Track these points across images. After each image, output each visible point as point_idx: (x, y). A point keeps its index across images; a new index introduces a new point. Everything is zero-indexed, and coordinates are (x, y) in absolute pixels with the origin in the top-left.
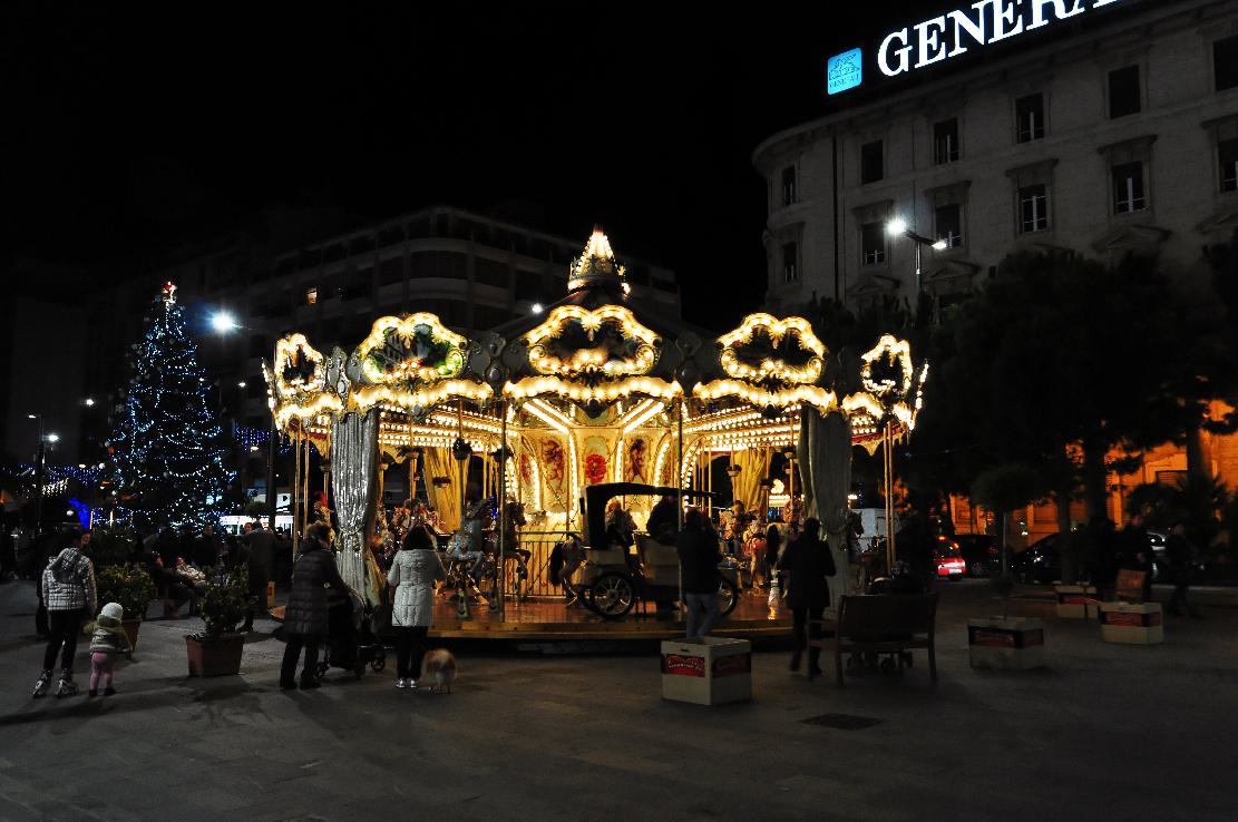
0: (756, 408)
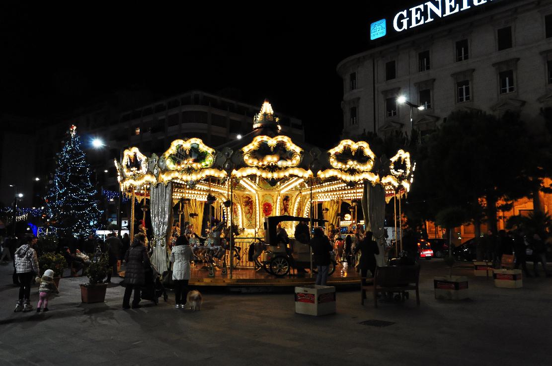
0: (344, 182)
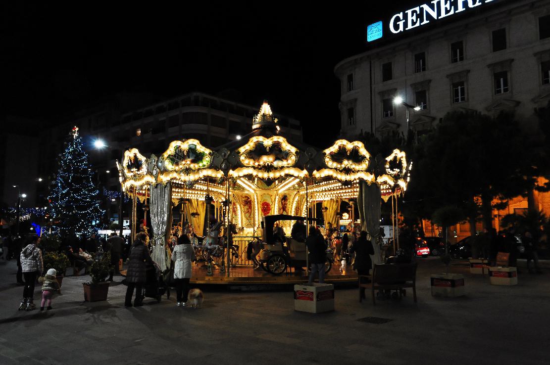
0: (340, 181)
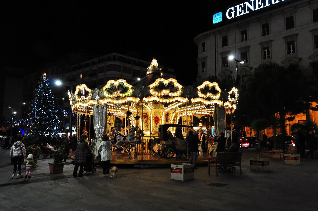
0: (204, 104)
